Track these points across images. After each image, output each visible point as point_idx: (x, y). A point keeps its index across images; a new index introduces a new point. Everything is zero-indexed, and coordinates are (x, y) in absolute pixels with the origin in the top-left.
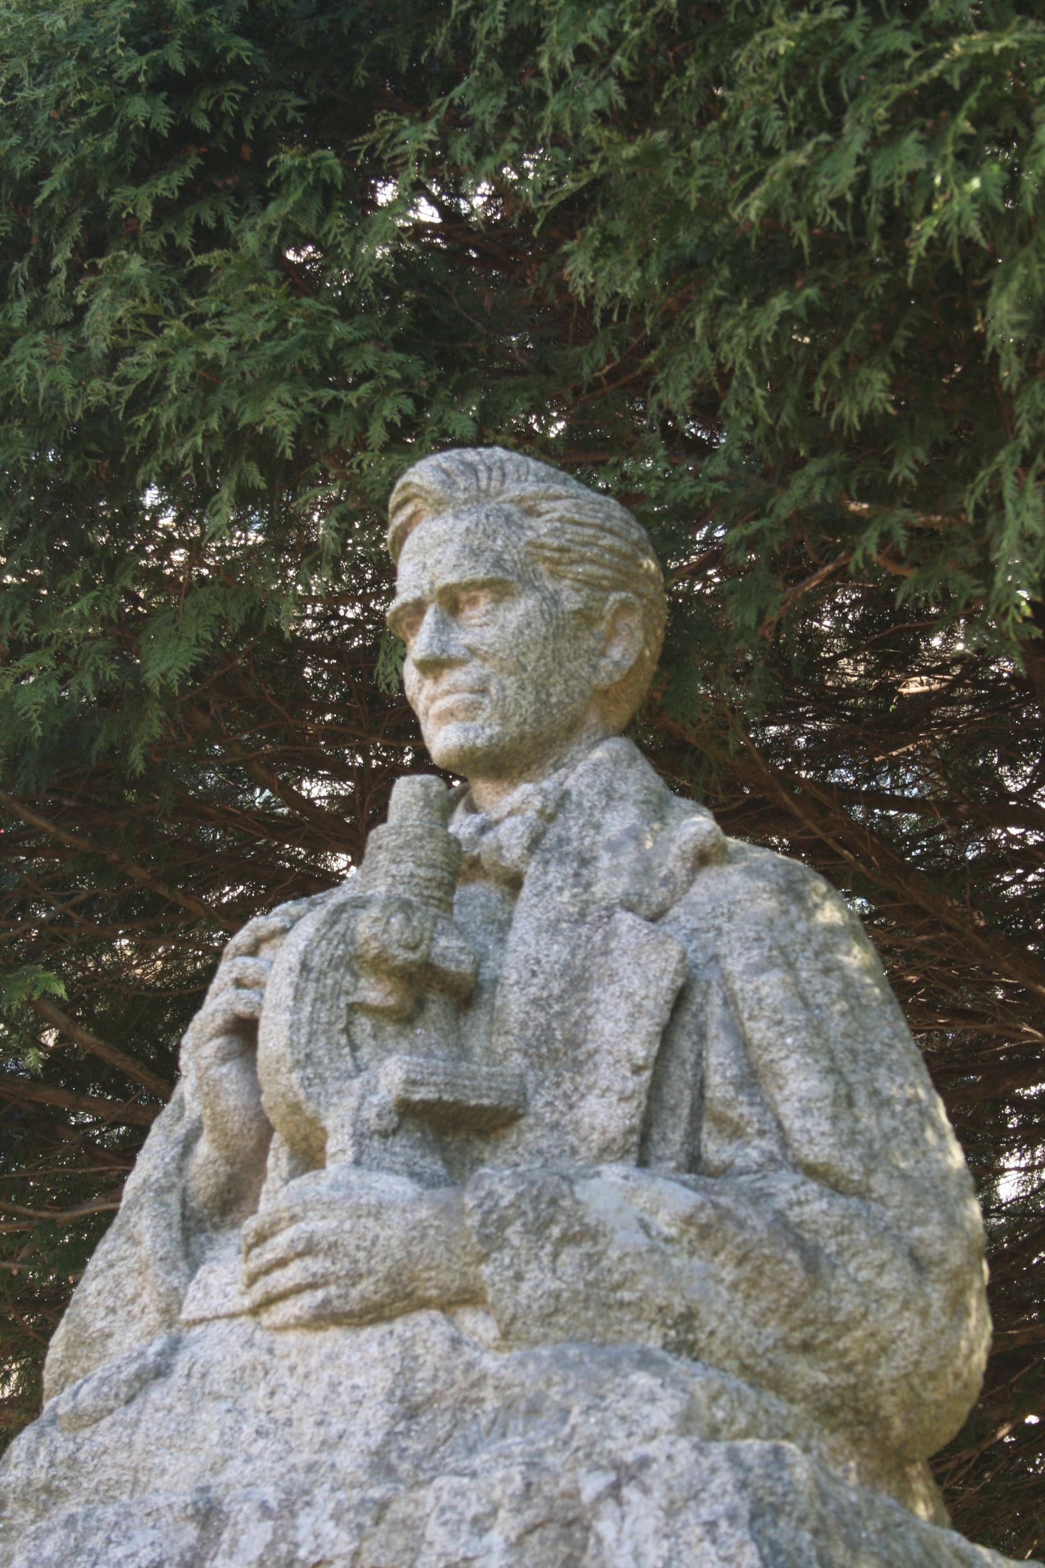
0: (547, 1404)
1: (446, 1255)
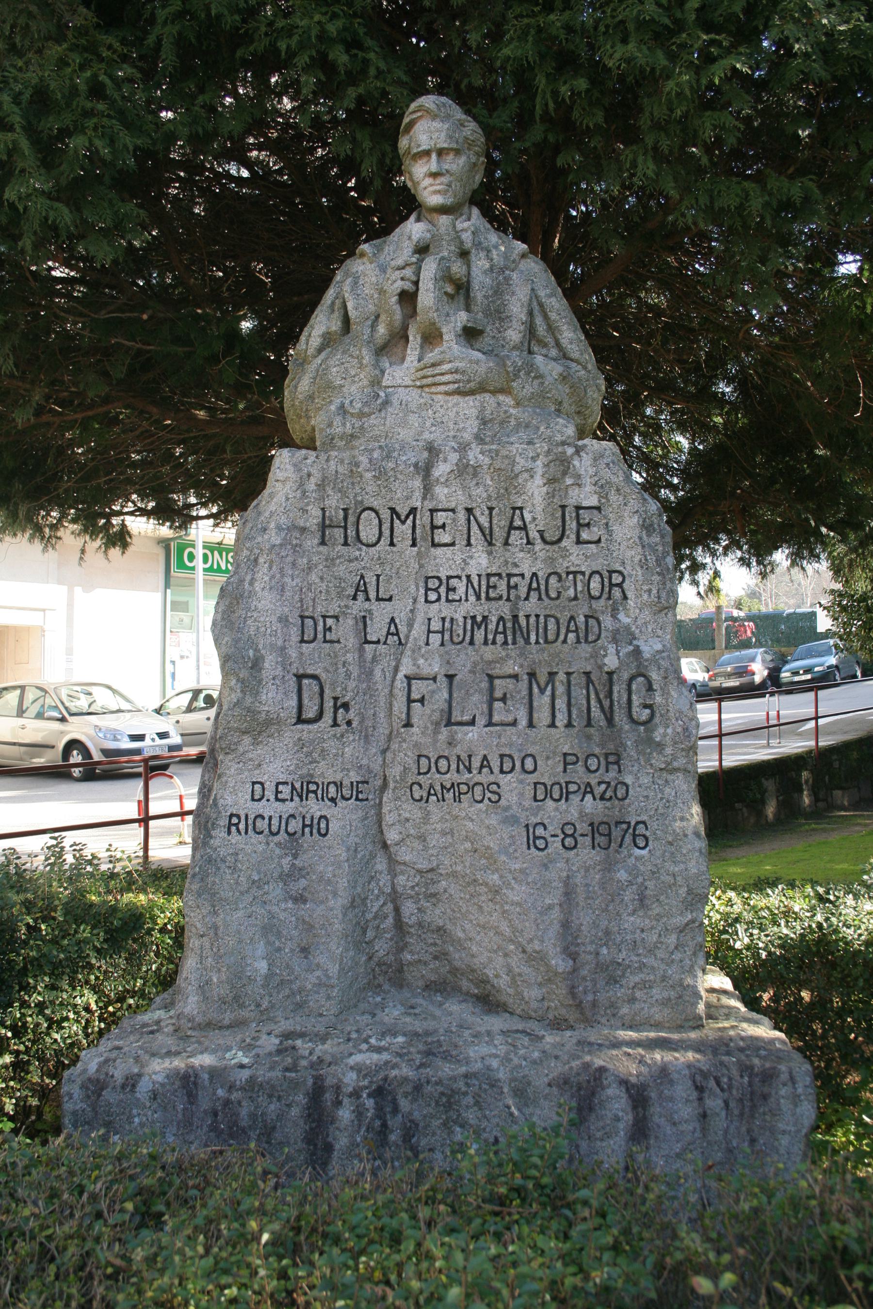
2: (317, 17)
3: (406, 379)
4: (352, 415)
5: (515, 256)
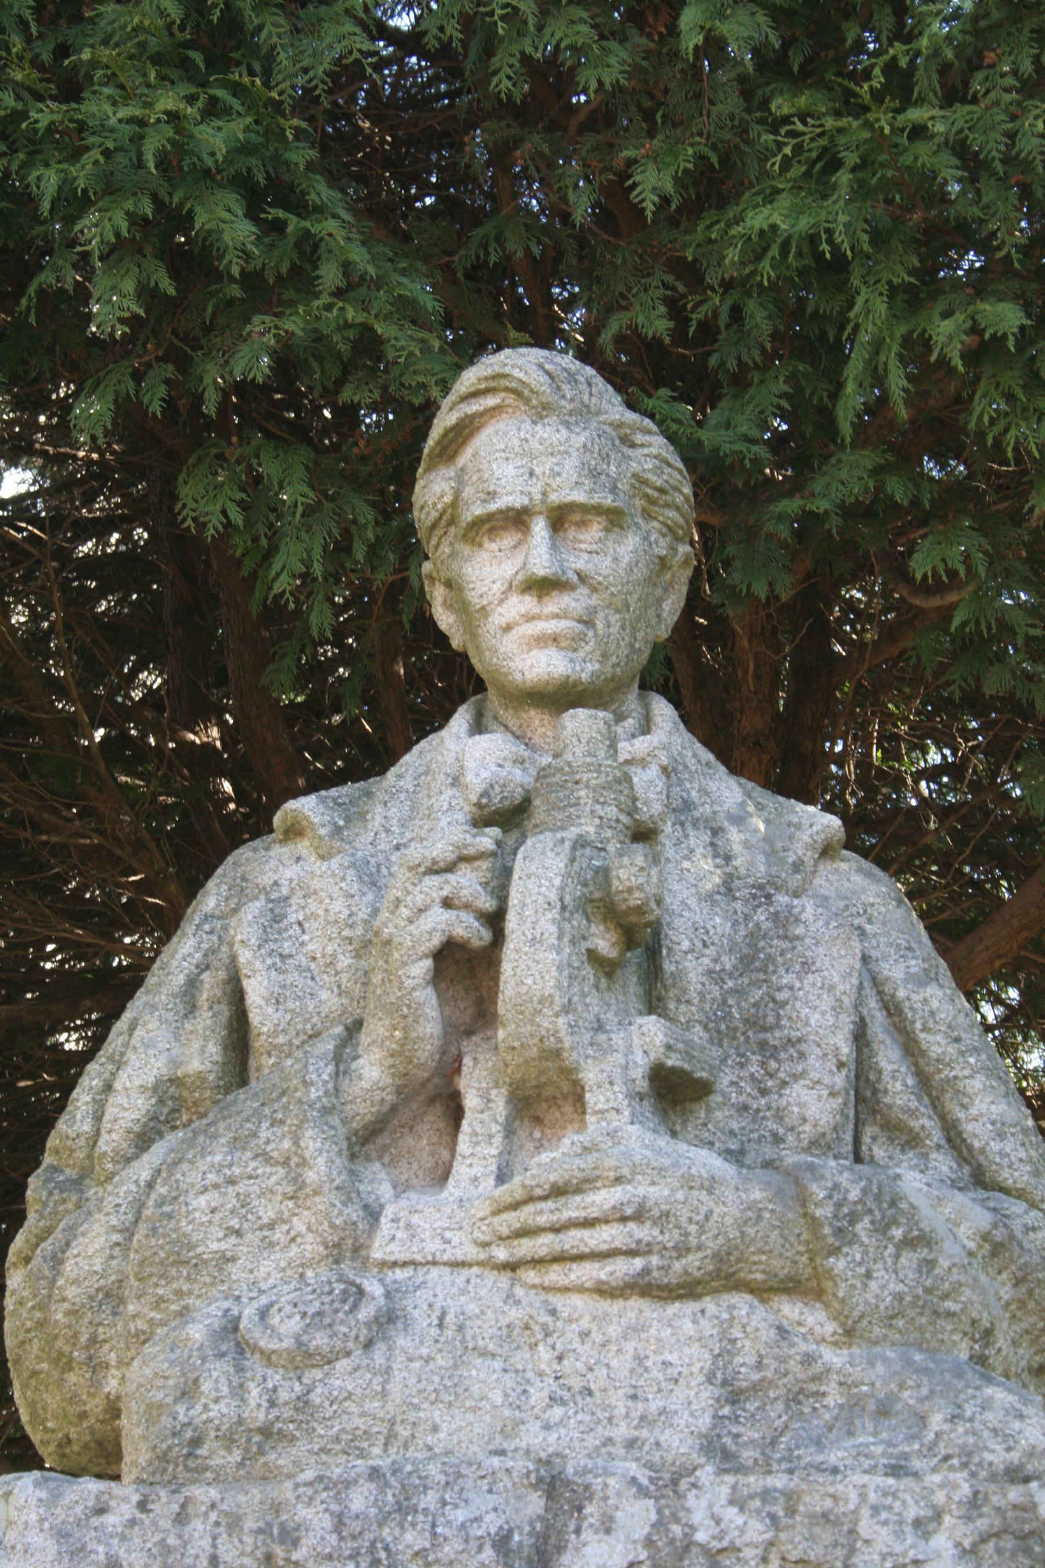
0: (899, 1406)
1: (780, 1241)
2: (167, 101)
3: (456, 1237)
4: (268, 1357)
5: (801, 847)
